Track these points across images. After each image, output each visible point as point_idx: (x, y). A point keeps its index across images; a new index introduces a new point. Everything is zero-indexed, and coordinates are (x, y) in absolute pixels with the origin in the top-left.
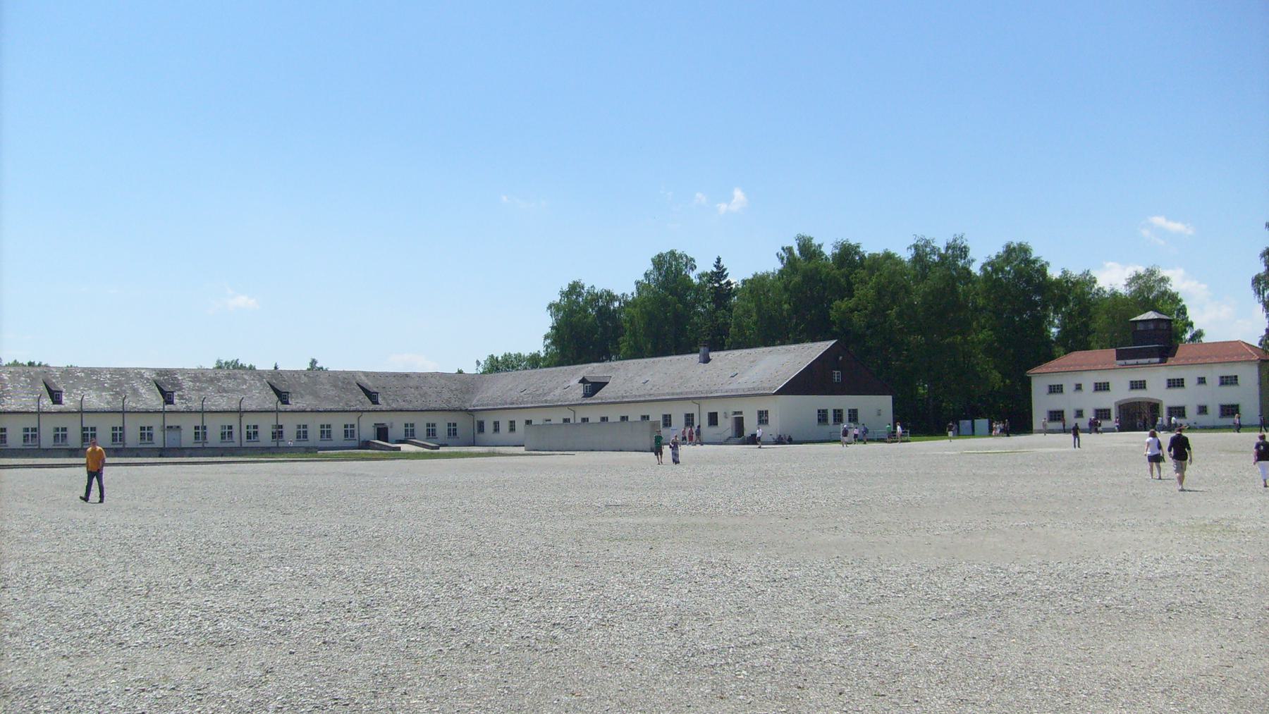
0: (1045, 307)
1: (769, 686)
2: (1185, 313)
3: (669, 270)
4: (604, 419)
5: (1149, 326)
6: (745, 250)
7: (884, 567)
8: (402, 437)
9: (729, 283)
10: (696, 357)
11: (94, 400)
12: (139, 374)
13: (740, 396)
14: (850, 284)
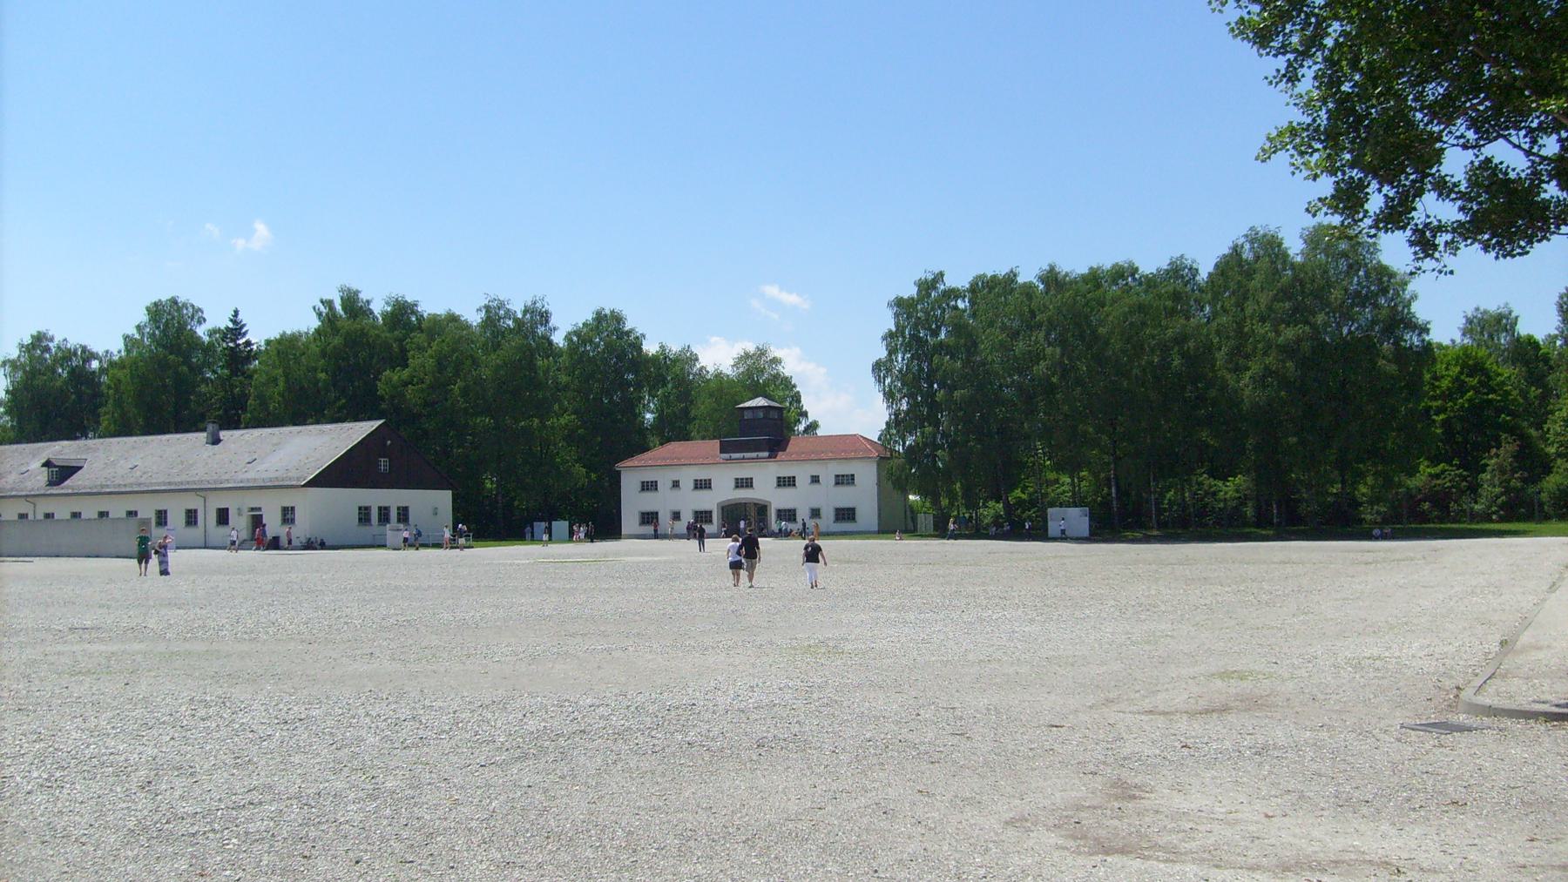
0: (639, 386)
1: (266, 857)
2: (799, 401)
3: (170, 323)
5: (759, 415)
6: (275, 306)
7: (427, 703)
9: (248, 343)
13: (261, 488)
14: (404, 351)
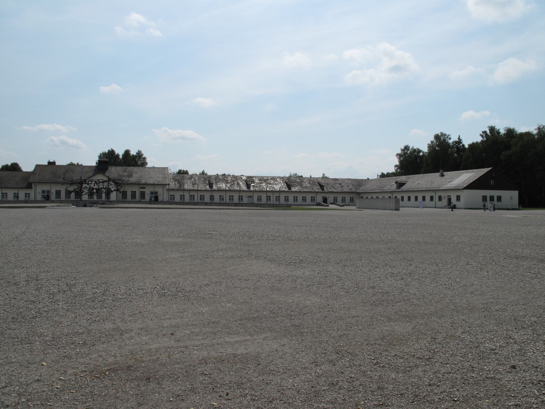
4: (390, 197)
8: (333, 202)
10: (438, 174)
11: (223, 186)
12: (240, 178)
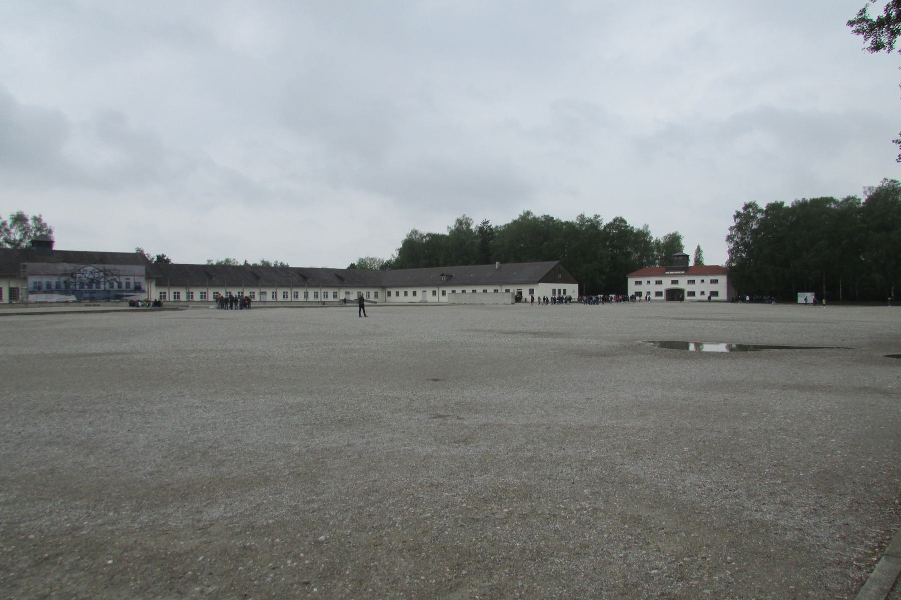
5: (671, 256)
